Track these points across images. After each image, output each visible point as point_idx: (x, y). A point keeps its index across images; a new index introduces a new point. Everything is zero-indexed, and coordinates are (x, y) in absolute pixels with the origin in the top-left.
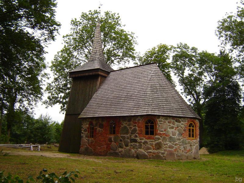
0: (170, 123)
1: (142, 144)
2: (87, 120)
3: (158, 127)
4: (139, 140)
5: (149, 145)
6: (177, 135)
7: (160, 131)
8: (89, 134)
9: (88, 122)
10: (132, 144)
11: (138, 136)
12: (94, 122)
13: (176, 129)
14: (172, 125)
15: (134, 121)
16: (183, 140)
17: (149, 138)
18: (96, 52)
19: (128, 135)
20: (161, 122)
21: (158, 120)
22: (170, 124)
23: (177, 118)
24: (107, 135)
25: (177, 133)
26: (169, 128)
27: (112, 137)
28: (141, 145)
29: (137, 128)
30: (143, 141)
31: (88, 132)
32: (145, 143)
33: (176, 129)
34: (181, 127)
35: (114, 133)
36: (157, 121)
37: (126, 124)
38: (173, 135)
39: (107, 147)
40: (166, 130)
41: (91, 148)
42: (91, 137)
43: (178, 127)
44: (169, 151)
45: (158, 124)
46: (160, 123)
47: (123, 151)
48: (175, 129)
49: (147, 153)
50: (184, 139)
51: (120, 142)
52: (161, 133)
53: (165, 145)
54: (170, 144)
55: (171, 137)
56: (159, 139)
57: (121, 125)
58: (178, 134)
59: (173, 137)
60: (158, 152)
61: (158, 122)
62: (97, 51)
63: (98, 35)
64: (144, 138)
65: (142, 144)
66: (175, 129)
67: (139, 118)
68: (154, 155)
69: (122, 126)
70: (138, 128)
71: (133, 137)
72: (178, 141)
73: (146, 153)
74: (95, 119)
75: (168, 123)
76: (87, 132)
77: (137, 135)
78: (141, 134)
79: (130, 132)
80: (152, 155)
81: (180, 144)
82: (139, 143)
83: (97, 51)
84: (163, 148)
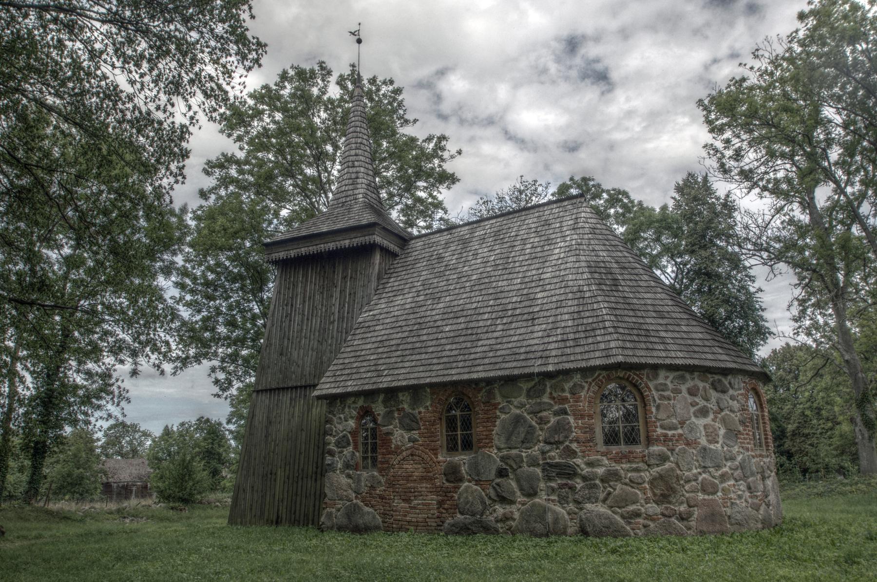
0: (696, 396)
1: (597, 482)
2: (350, 401)
3: (654, 410)
4: (583, 466)
5: (626, 484)
6: (721, 440)
7: (662, 427)
8: (357, 454)
9: (355, 409)
10: (553, 484)
11: (578, 450)
12: (379, 409)
13: (716, 417)
14: (702, 403)
15: (555, 395)
16: (744, 460)
17: (620, 458)
18: (357, 178)
19: (535, 451)
20: (663, 390)
21: (651, 385)
22: (697, 400)
23: (717, 377)
24: (436, 454)
25: (722, 432)
26: (694, 413)
27: (462, 459)
28: (595, 486)
29: (571, 419)
30: (600, 471)
31: (356, 447)
32: (611, 476)
33: (716, 417)
34: (731, 411)
35: (468, 445)
36: (650, 390)
37: (522, 406)
38: (710, 442)
39: (440, 503)
40: (684, 423)
41: (371, 510)
42: (365, 468)
43: (722, 410)
44: (705, 503)
45: (654, 401)
46: (662, 397)
47: (517, 515)
48: (711, 416)
49: (623, 517)
50: (747, 454)
51: (498, 480)
52: (670, 433)
53: (688, 481)
54: (704, 475)
55: (705, 449)
56: (663, 459)
57: (498, 413)
58: (726, 436)
59: (710, 449)
60: (666, 513)
61: (654, 392)
62: (361, 175)
63: (358, 123)
64: (604, 458)
65: (597, 482)
66: (711, 416)
67: (577, 378)
68: (652, 525)
69: (503, 416)
70: (575, 419)
71: (555, 455)
72: (729, 464)
73: (618, 518)
74: (382, 397)
75: (687, 396)
76: (351, 448)
77: (574, 446)
78: (589, 441)
79: (542, 435)
80: (645, 526)
81: (736, 474)
82: (584, 478)
83: (361, 175)
84: (683, 495)
